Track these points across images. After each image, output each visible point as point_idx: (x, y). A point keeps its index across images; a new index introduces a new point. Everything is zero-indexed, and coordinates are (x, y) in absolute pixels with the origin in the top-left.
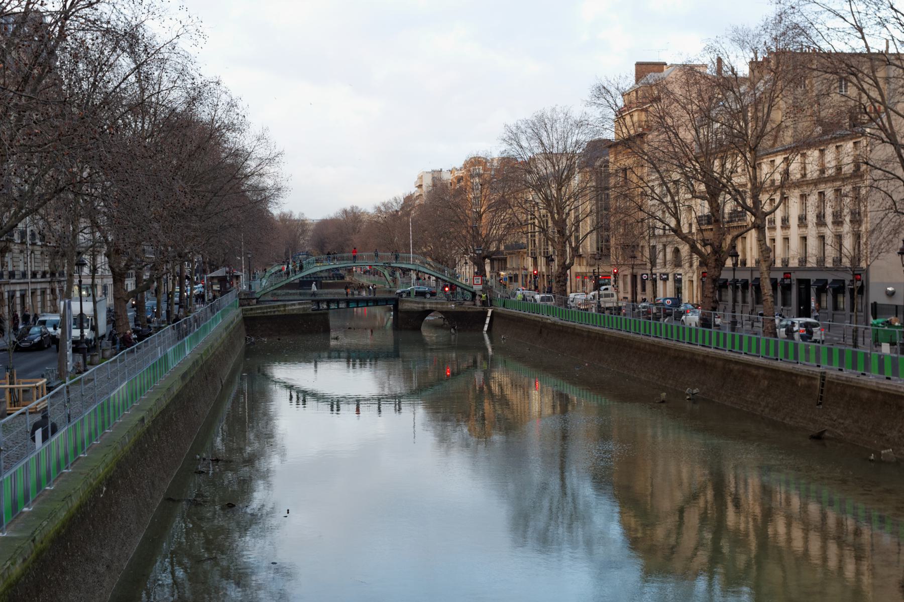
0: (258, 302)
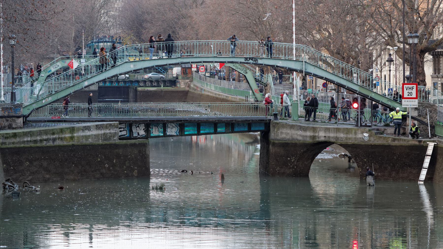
0: (26, 123)
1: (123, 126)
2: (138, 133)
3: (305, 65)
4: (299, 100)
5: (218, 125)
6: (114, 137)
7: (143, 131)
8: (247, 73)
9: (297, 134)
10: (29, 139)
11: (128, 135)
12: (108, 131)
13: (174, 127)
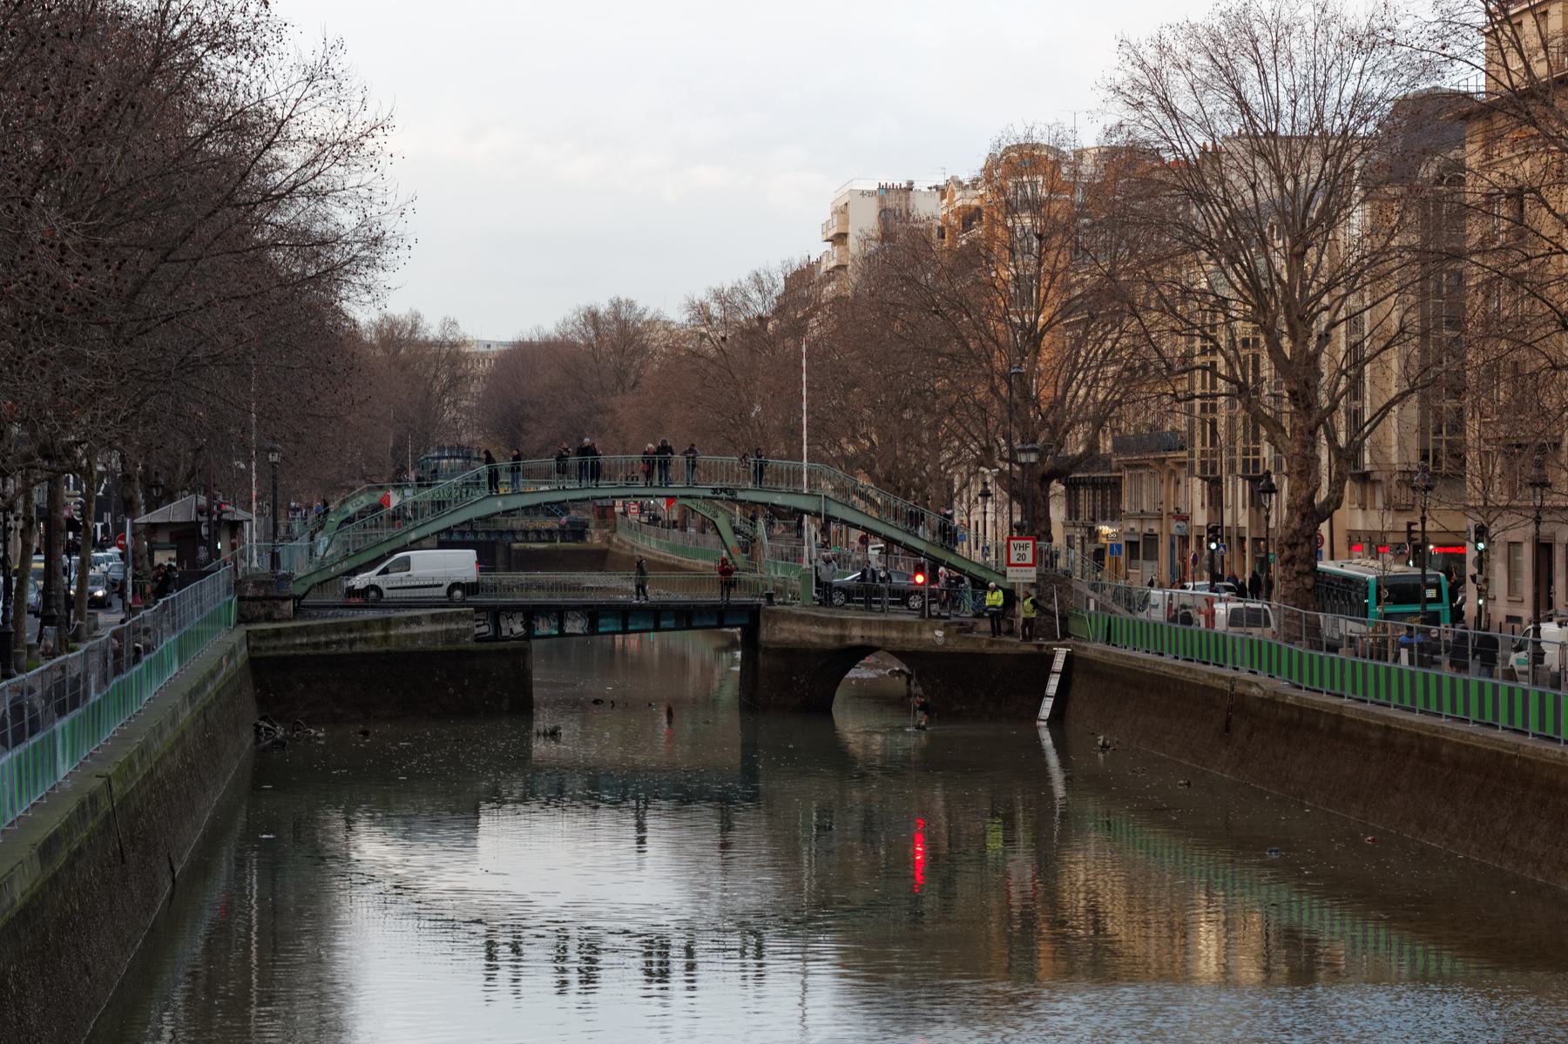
0: (299, 611)
6: (465, 636)
10: (305, 640)
12: (453, 626)
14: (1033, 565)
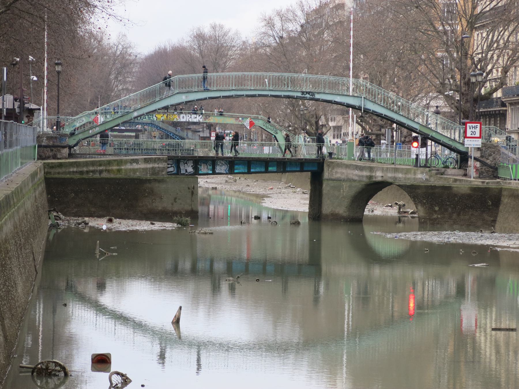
0: (71, 155)
1: (171, 162)
2: (186, 170)
3: (364, 101)
4: (354, 139)
5: (270, 164)
6: (162, 172)
7: (191, 168)
8: (277, 133)
9: (352, 174)
10: (75, 170)
11: (175, 172)
12: (156, 165)
13: (223, 165)
14: (480, 138)
